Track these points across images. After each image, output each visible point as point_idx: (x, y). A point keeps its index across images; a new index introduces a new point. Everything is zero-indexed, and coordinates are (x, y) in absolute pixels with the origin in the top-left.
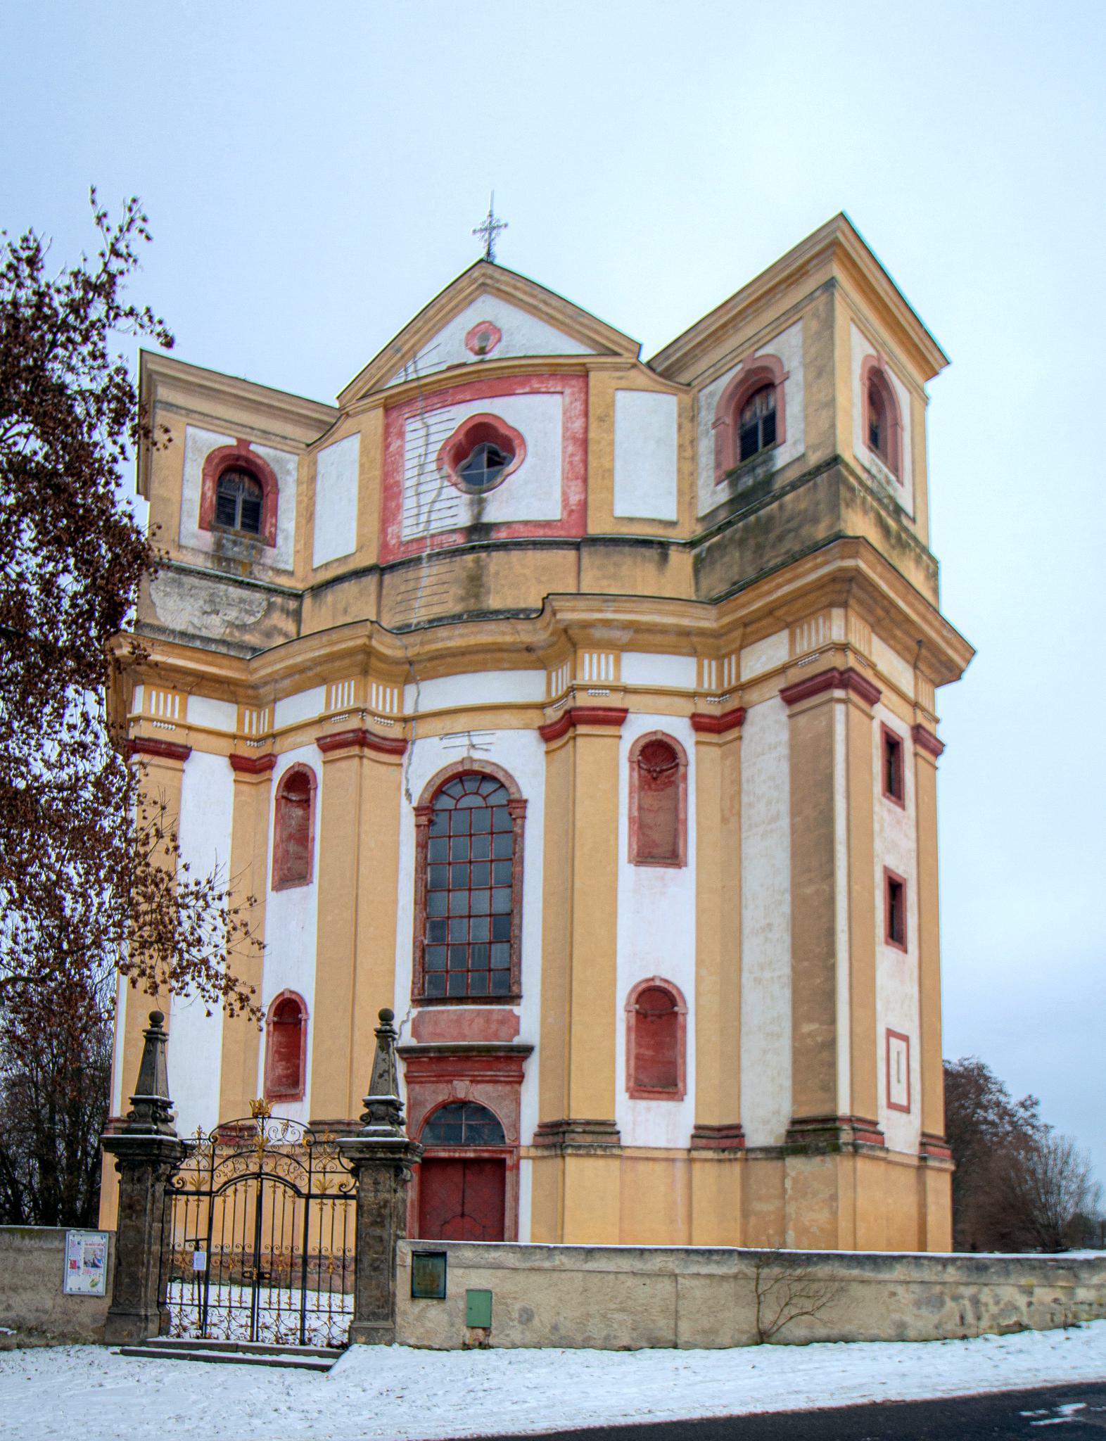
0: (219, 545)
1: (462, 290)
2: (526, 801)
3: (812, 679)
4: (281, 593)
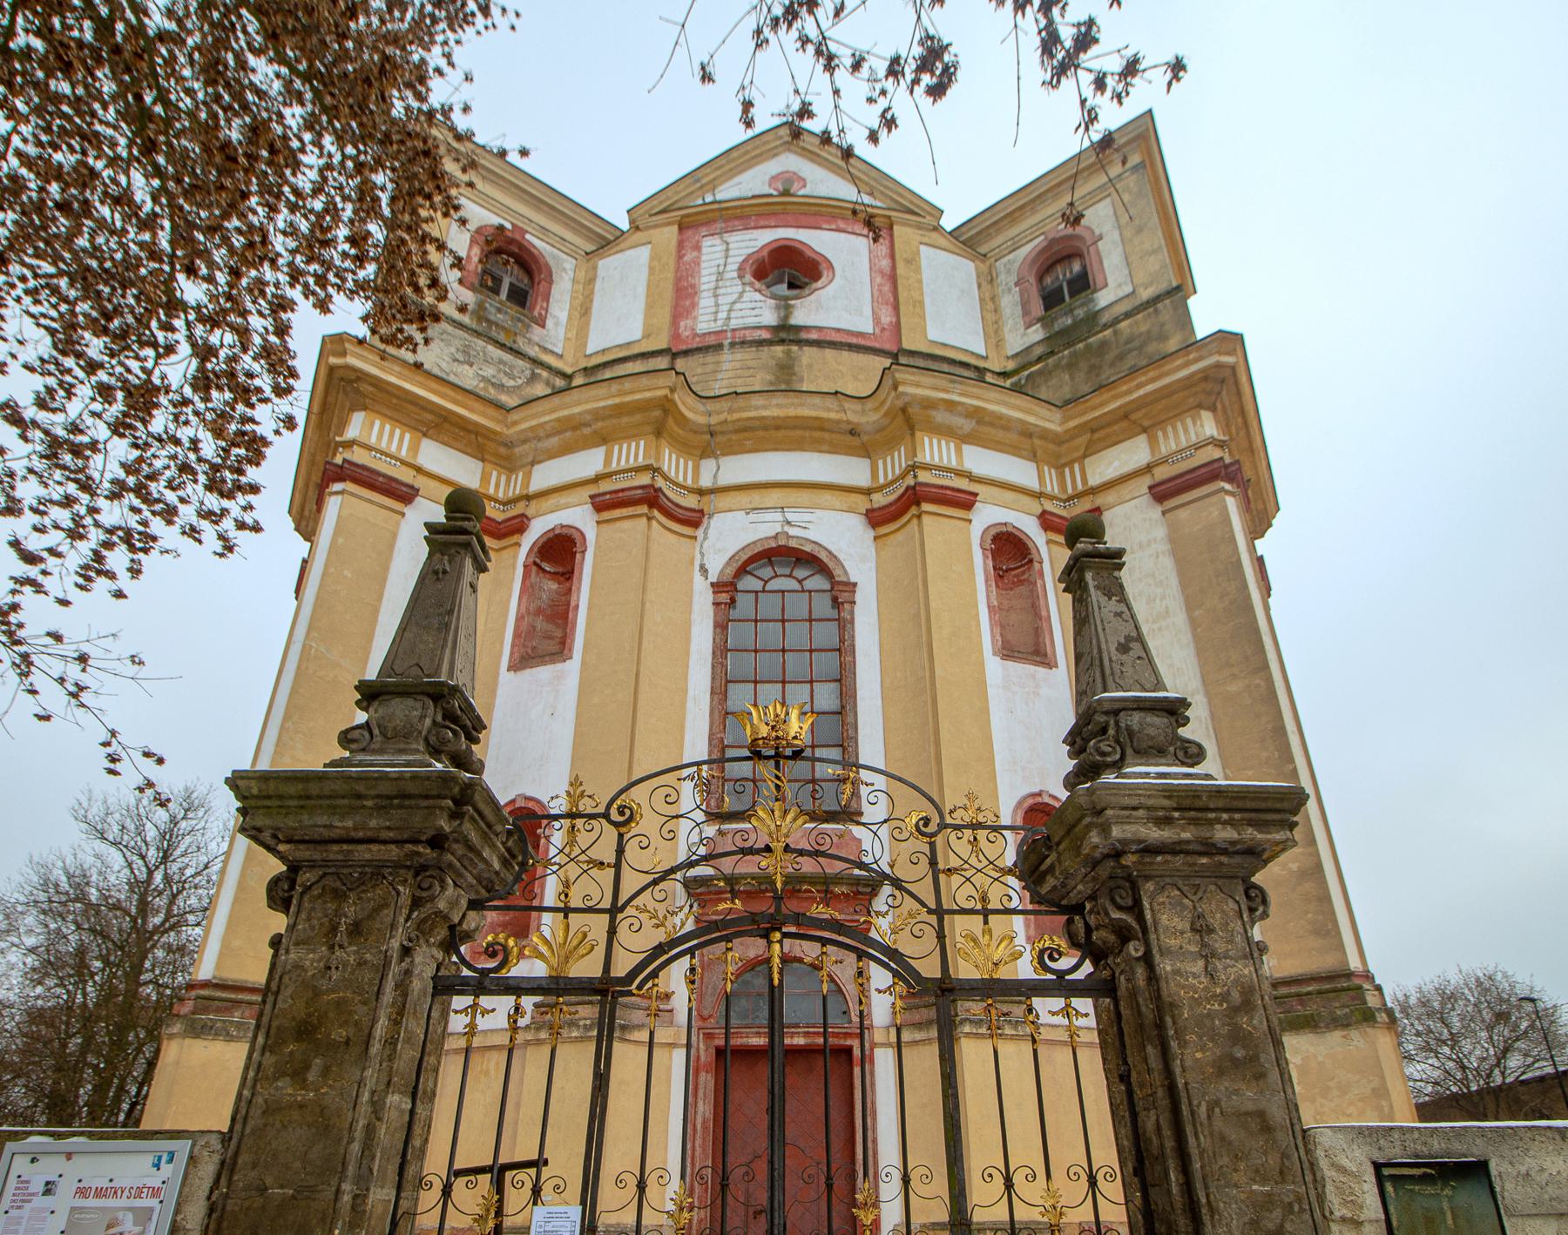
0: (480, 306)
2: (855, 585)
4: (549, 368)
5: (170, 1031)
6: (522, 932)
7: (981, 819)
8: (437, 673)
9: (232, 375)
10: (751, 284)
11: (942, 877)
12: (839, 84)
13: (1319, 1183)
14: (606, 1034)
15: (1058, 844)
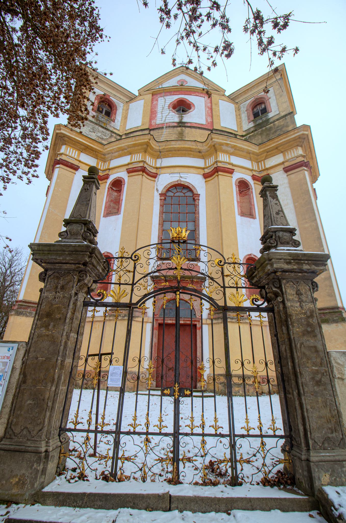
0: (97, 116)
1: (177, 71)
2: (199, 195)
3: (292, 165)
4: (116, 133)
5: (11, 313)
6: (106, 289)
7: (236, 261)
8: (85, 217)
9: (32, 135)
10: (172, 110)
11: (225, 277)
12: (199, 55)
13: (332, 367)
14: (131, 319)
15: (258, 269)
